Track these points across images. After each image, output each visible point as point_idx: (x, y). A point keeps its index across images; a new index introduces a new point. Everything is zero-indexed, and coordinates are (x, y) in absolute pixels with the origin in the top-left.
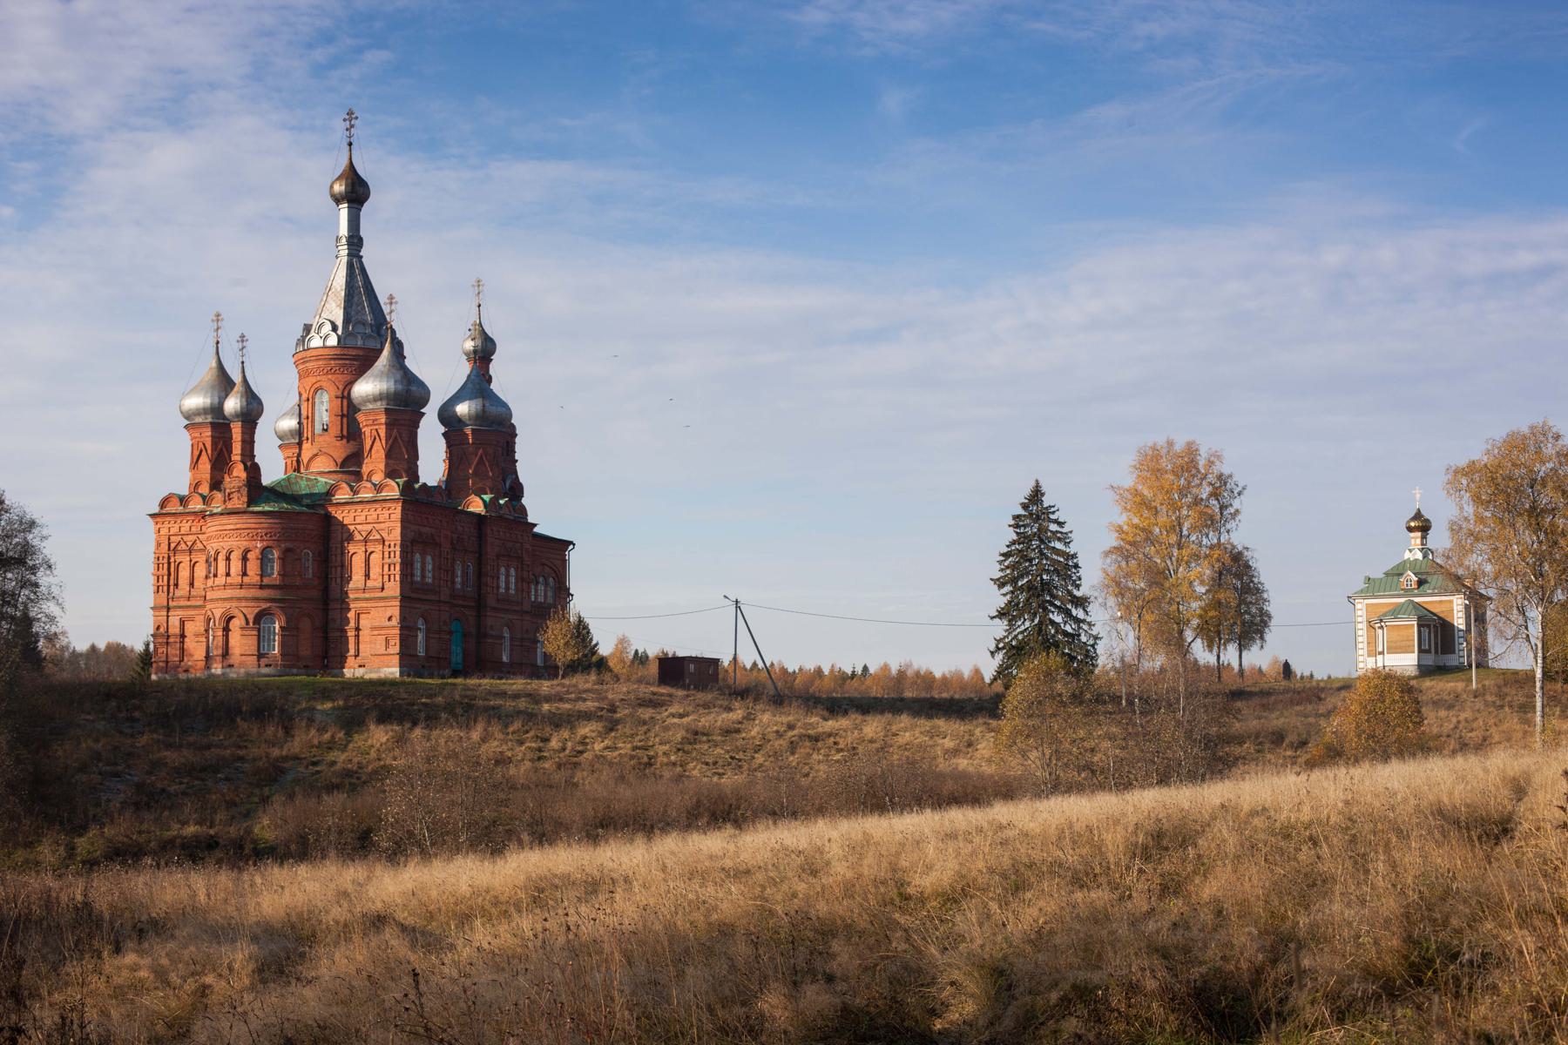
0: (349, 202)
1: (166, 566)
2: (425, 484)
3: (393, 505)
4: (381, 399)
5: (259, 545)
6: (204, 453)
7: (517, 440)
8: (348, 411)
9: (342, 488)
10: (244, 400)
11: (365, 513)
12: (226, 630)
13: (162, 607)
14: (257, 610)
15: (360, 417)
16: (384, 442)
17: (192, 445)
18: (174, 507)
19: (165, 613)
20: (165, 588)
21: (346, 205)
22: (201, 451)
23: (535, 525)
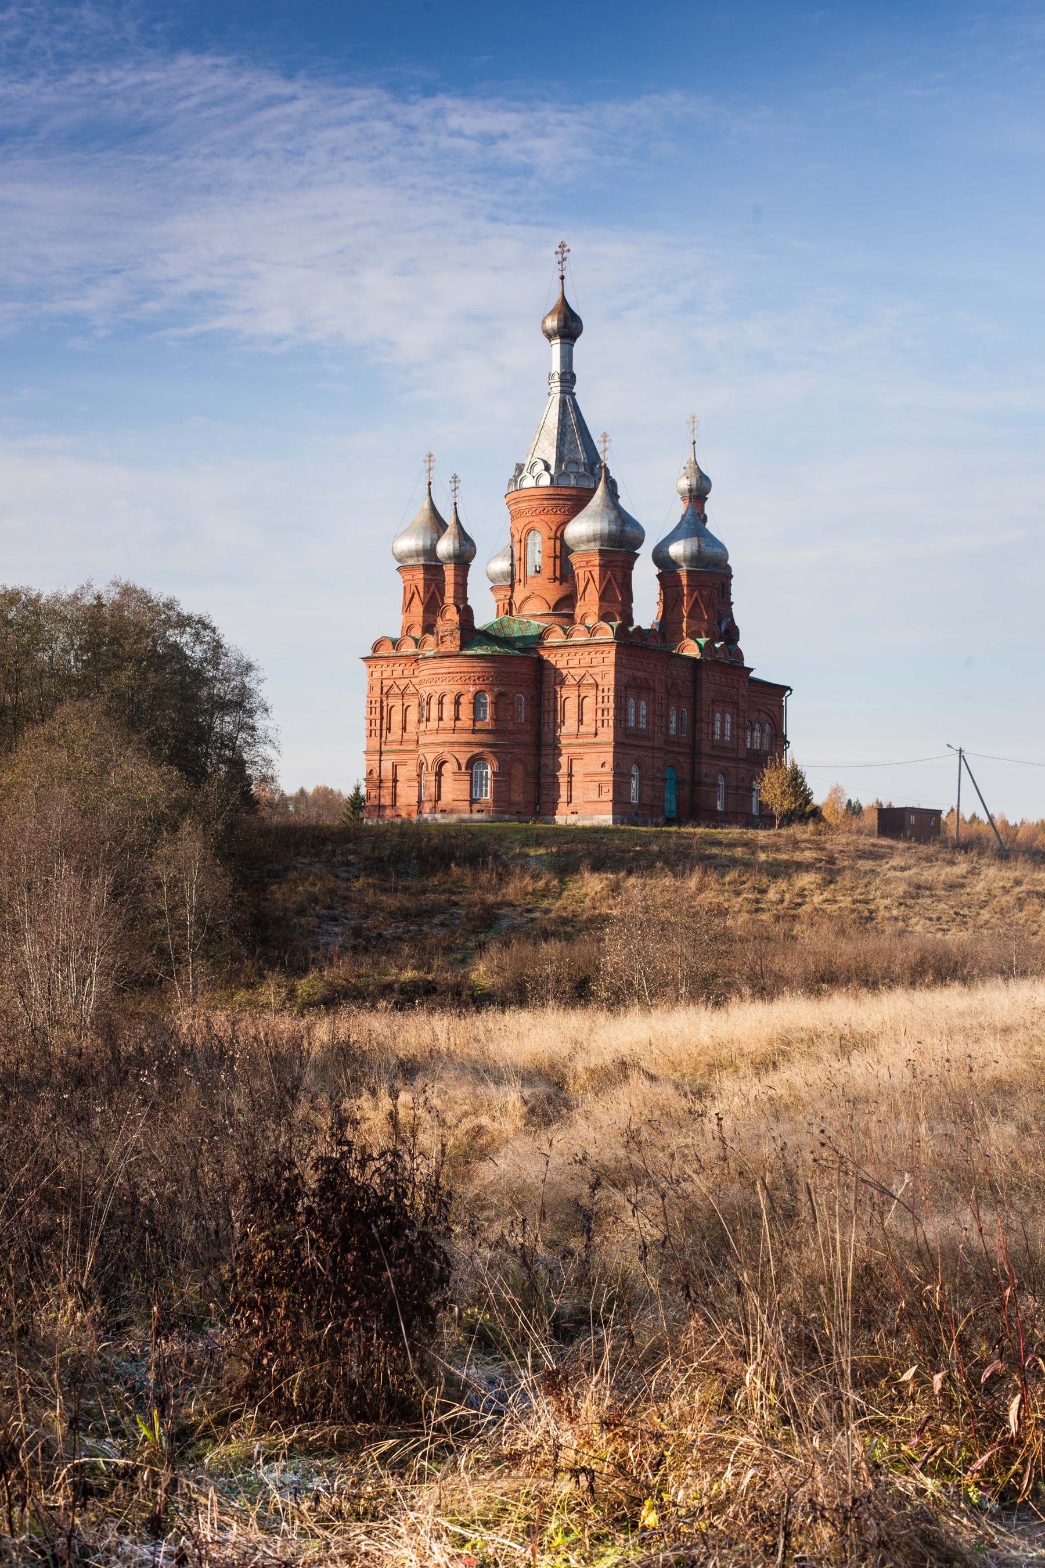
0: (561, 337)
1: (378, 709)
2: (639, 628)
3: (607, 649)
4: (595, 540)
7: (733, 581)
10: (457, 541)
11: (578, 657)
14: (469, 755)
15: (573, 558)
16: (597, 584)
18: (386, 650)
20: (378, 732)
21: (559, 341)
22: (414, 594)
23: (751, 670)
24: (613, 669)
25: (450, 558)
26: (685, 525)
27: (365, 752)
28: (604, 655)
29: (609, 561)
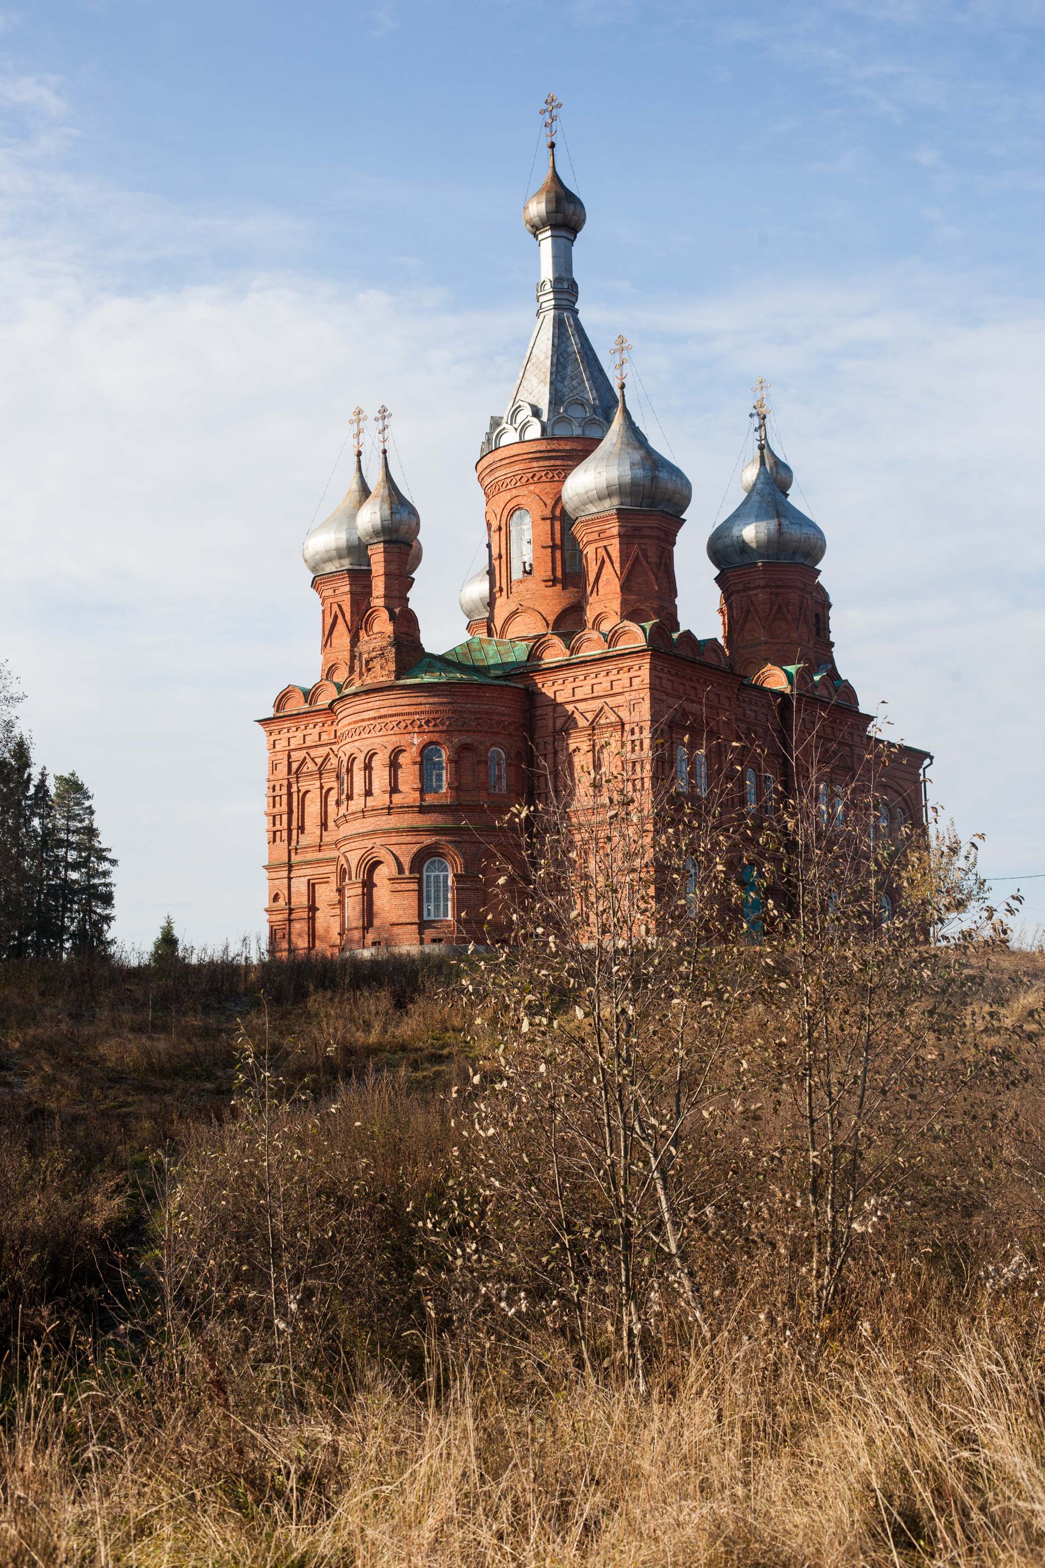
0: (554, 227)
1: (285, 798)
2: (688, 634)
3: (635, 662)
4: (610, 495)
5: (416, 741)
6: (340, 619)
7: (832, 613)
8: (562, 540)
9: (553, 646)
10: (386, 506)
11: (590, 681)
12: (368, 885)
13: (279, 866)
14: (415, 848)
15: (579, 531)
16: (617, 566)
17: (323, 611)
18: (296, 705)
19: (285, 874)
20: (285, 834)
21: (549, 233)
22: (336, 617)
24: (646, 694)
25: (376, 533)
26: (756, 498)
27: (266, 867)
28: (632, 674)
29: (635, 529)
